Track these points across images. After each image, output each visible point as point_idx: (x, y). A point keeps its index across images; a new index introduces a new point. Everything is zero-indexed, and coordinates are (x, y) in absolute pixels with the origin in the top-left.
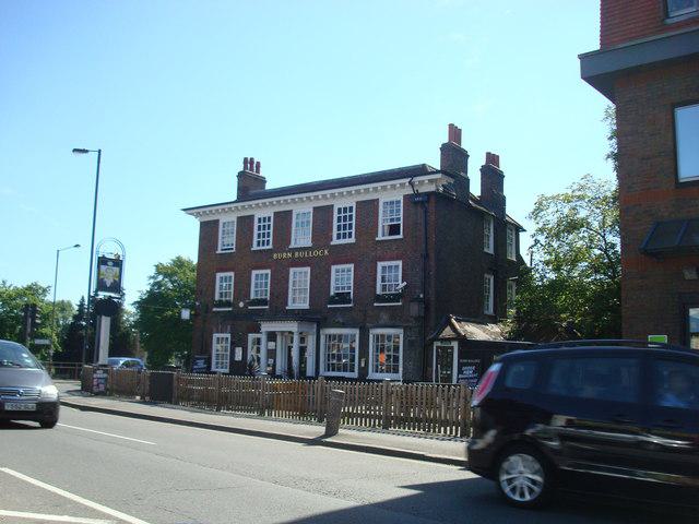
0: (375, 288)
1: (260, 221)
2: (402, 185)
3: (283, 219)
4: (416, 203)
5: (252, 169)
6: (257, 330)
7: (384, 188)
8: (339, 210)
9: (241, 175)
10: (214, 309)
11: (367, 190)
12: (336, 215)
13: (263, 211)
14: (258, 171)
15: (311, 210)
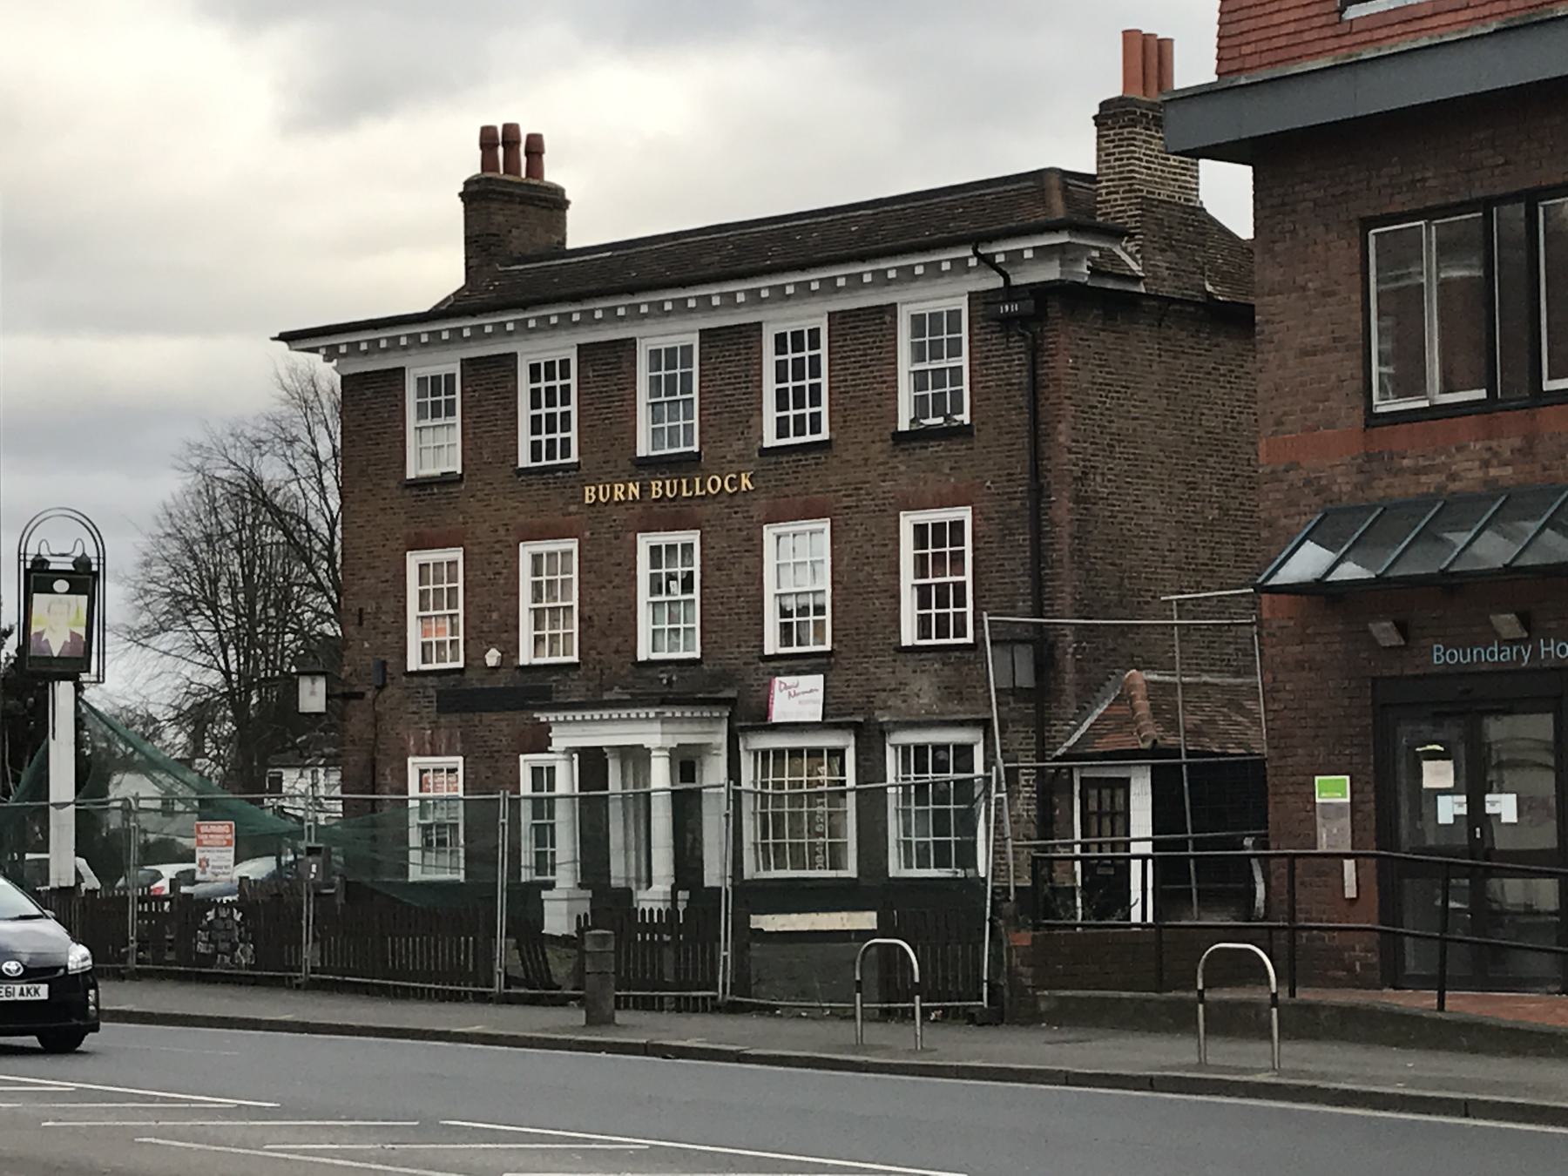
0: (761, 636)
1: (535, 377)
2: (960, 265)
3: (608, 364)
4: (1007, 322)
5: (511, 165)
6: (542, 745)
7: (779, 294)
8: (780, 339)
9: (475, 194)
10: (917, 979)
11: (855, 281)
12: (524, 387)
13: (545, 345)
14: (535, 166)
15: (695, 340)
